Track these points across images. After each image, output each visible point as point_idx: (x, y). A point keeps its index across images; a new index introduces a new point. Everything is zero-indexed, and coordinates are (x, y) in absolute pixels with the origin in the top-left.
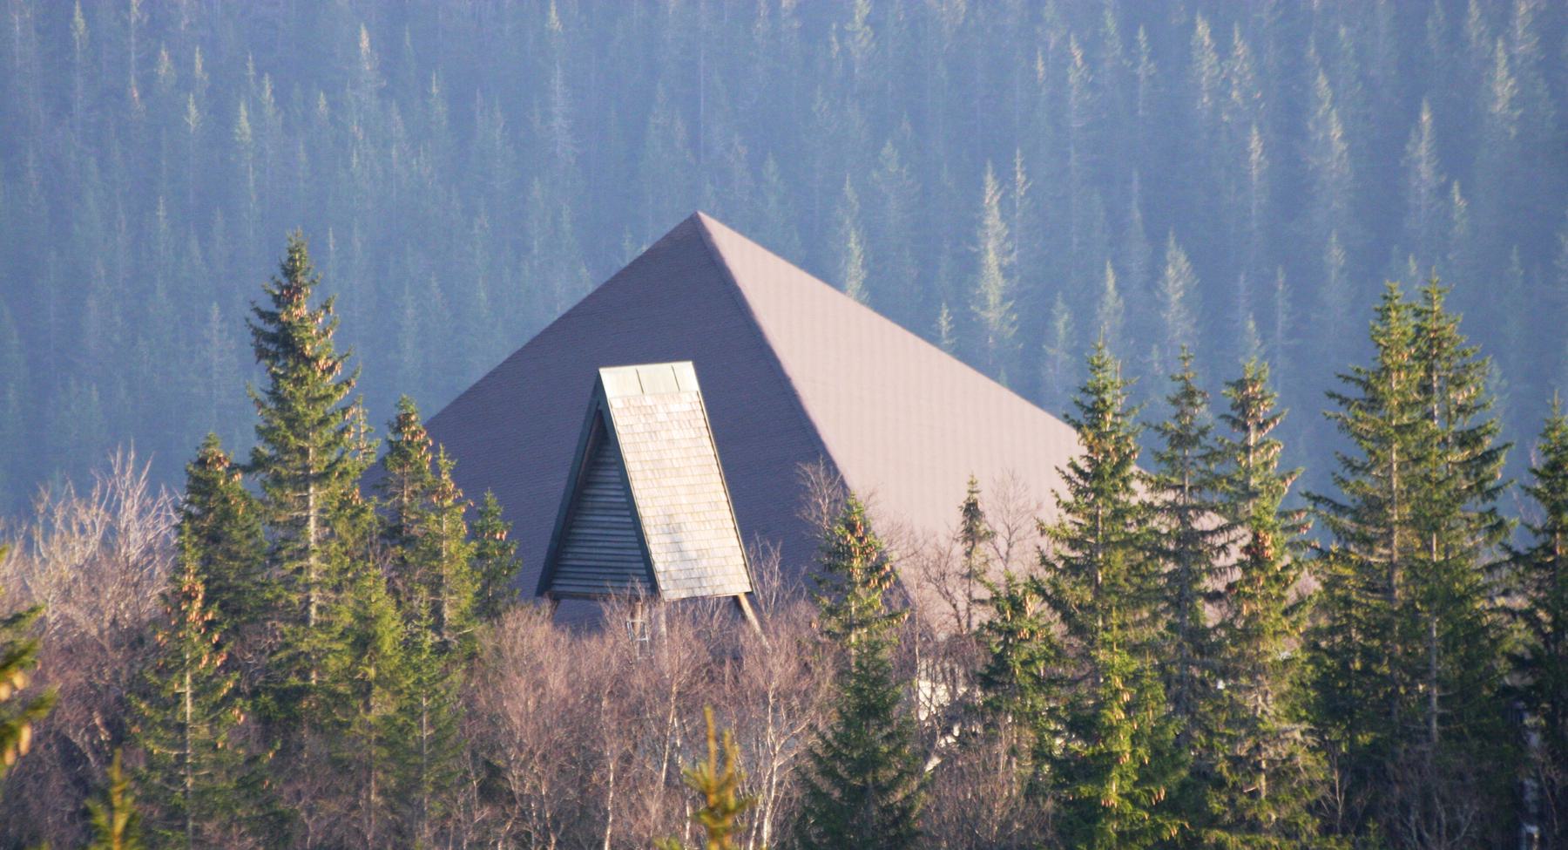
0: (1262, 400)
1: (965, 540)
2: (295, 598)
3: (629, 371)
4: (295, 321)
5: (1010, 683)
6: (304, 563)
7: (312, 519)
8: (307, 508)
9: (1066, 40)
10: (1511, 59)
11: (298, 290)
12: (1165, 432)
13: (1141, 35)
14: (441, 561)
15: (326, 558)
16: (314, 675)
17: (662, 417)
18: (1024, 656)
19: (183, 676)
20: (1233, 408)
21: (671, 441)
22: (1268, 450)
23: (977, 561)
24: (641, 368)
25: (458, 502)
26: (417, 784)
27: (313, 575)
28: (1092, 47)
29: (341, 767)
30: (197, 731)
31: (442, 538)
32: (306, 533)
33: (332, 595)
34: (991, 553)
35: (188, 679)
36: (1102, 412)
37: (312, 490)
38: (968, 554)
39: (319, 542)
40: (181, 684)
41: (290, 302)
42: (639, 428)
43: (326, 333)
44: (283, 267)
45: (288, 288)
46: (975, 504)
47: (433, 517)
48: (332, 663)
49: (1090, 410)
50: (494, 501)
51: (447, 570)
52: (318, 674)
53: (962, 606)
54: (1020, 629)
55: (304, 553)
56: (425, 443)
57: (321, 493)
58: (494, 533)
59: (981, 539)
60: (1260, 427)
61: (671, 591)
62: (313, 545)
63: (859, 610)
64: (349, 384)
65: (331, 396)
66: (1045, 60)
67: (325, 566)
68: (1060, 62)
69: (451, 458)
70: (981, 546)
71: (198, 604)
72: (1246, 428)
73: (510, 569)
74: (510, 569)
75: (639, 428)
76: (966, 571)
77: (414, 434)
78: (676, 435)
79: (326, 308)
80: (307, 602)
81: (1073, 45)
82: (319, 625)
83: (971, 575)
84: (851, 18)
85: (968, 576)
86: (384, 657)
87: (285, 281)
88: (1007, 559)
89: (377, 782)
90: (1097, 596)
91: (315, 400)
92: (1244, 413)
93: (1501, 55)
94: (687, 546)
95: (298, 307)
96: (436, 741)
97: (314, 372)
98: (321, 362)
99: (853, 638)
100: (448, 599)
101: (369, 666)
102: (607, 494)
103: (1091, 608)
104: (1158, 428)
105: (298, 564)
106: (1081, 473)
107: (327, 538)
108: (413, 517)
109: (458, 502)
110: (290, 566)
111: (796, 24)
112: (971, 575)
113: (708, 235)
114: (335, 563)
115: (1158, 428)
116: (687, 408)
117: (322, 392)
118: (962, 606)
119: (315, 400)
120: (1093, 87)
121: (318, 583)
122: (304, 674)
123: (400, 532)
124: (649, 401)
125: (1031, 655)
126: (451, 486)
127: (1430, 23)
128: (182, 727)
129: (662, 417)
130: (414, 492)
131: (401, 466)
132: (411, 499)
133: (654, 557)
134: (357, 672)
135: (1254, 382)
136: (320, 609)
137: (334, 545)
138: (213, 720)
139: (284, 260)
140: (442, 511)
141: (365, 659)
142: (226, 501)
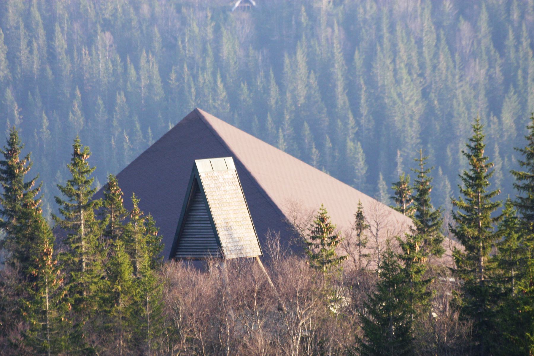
0: (408, 190)
1: (357, 229)
2: (76, 260)
3: (207, 161)
4: (15, 164)
5: (410, 281)
6: (80, 244)
7: (82, 225)
8: (80, 220)
9: (122, 133)
10: (284, 136)
11: (15, 151)
12: (525, 152)
13: (149, 131)
14: (135, 243)
15: (89, 242)
16: (85, 293)
17: (221, 180)
18: (415, 270)
19: (45, 289)
20: (396, 194)
21: (225, 191)
22: (411, 211)
23: (362, 237)
24: (212, 160)
25: (141, 217)
26: (144, 335)
27: (84, 249)
28: (131, 134)
29: (108, 330)
30: (51, 314)
31: (135, 233)
32: (81, 231)
33: (92, 258)
34: (369, 234)
35: (47, 291)
36: (479, 149)
37: (82, 212)
38: (358, 235)
39: (85, 235)
40: (44, 293)
41: (12, 157)
42: (212, 185)
43: (27, 169)
44: (8, 142)
45: (11, 151)
46: (361, 213)
47: (131, 224)
48: (93, 287)
49: (473, 149)
50: (152, 218)
51: (137, 247)
52: (87, 293)
53: (357, 257)
54: (414, 257)
55: (80, 240)
56: (120, 194)
57: (85, 214)
58: (153, 232)
59: (364, 228)
60: (408, 201)
61: (230, 255)
62: (83, 236)
63: (327, 256)
64: (38, 190)
65: (89, 171)
66: (114, 140)
67: (88, 245)
68: (120, 140)
69: (138, 198)
70: (364, 232)
71: (50, 257)
72: (401, 202)
73: (160, 248)
74: (160, 248)
75: (212, 185)
76: (357, 243)
77: (116, 190)
78: (227, 188)
79: (27, 158)
80: (81, 261)
81: (125, 134)
82: (87, 271)
83: (360, 244)
84: (41, 127)
85: (359, 245)
86: (125, 281)
87: (9, 148)
88: (376, 236)
89: (123, 336)
90: (479, 232)
91: (82, 173)
92: (401, 196)
93: (281, 134)
94: (235, 235)
95: (15, 158)
96: (152, 317)
97: (82, 161)
98: (85, 156)
99: (325, 268)
100: (138, 260)
101: (118, 285)
102: (201, 214)
103: (477, 238)
104: (521, 150)
105: (77, 245)
106: (470, 178)
107: (88, 232)
108: (116, 226)
109: (141, 217)
110: (74, 246)
111: (21, 130)
112: (360, 244)
113: (203, 117)
114: (93, 243)
115: (521, 150)
116: (231, 177)
117: (85, 170)
118: (357, 257)
119: (82, 173)
120: (133, 150)
121: (86, 253)
122: (81, 293)
123: (111, 233)
124: (216, 174)
125: (418, 269)
126: (138, 210)
127: (253, 124)
128: (45, 312)
129: (221, 180)
130: (116, 216)
131: (111, 204)
132: (115, 219)
133: (221, 240)
134: (113, 288)
135: (404, 183)
136: (87, 265)
137: (92, 236)
138: (59, 309)
139: (8, 139)
140: (134, 222)
141: (117, 282)
142: (36, 221)
